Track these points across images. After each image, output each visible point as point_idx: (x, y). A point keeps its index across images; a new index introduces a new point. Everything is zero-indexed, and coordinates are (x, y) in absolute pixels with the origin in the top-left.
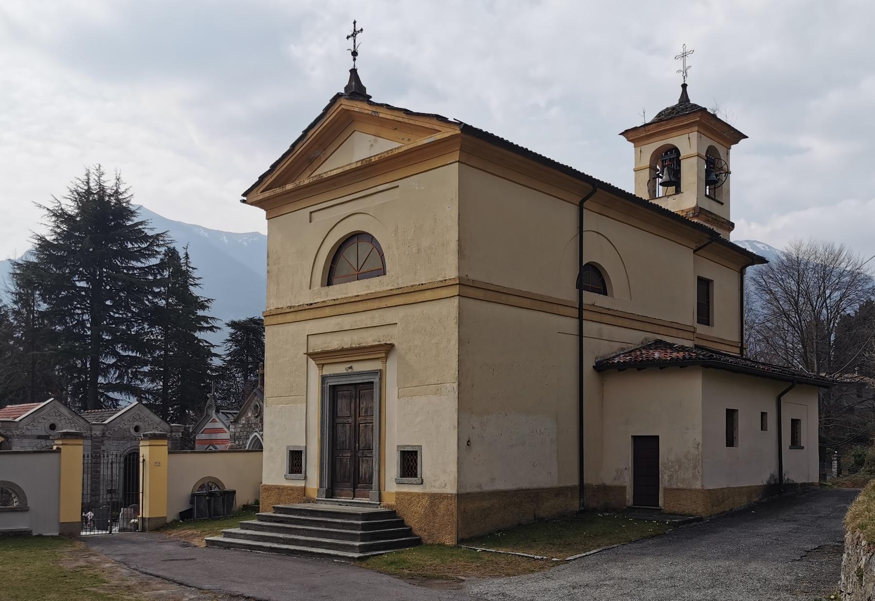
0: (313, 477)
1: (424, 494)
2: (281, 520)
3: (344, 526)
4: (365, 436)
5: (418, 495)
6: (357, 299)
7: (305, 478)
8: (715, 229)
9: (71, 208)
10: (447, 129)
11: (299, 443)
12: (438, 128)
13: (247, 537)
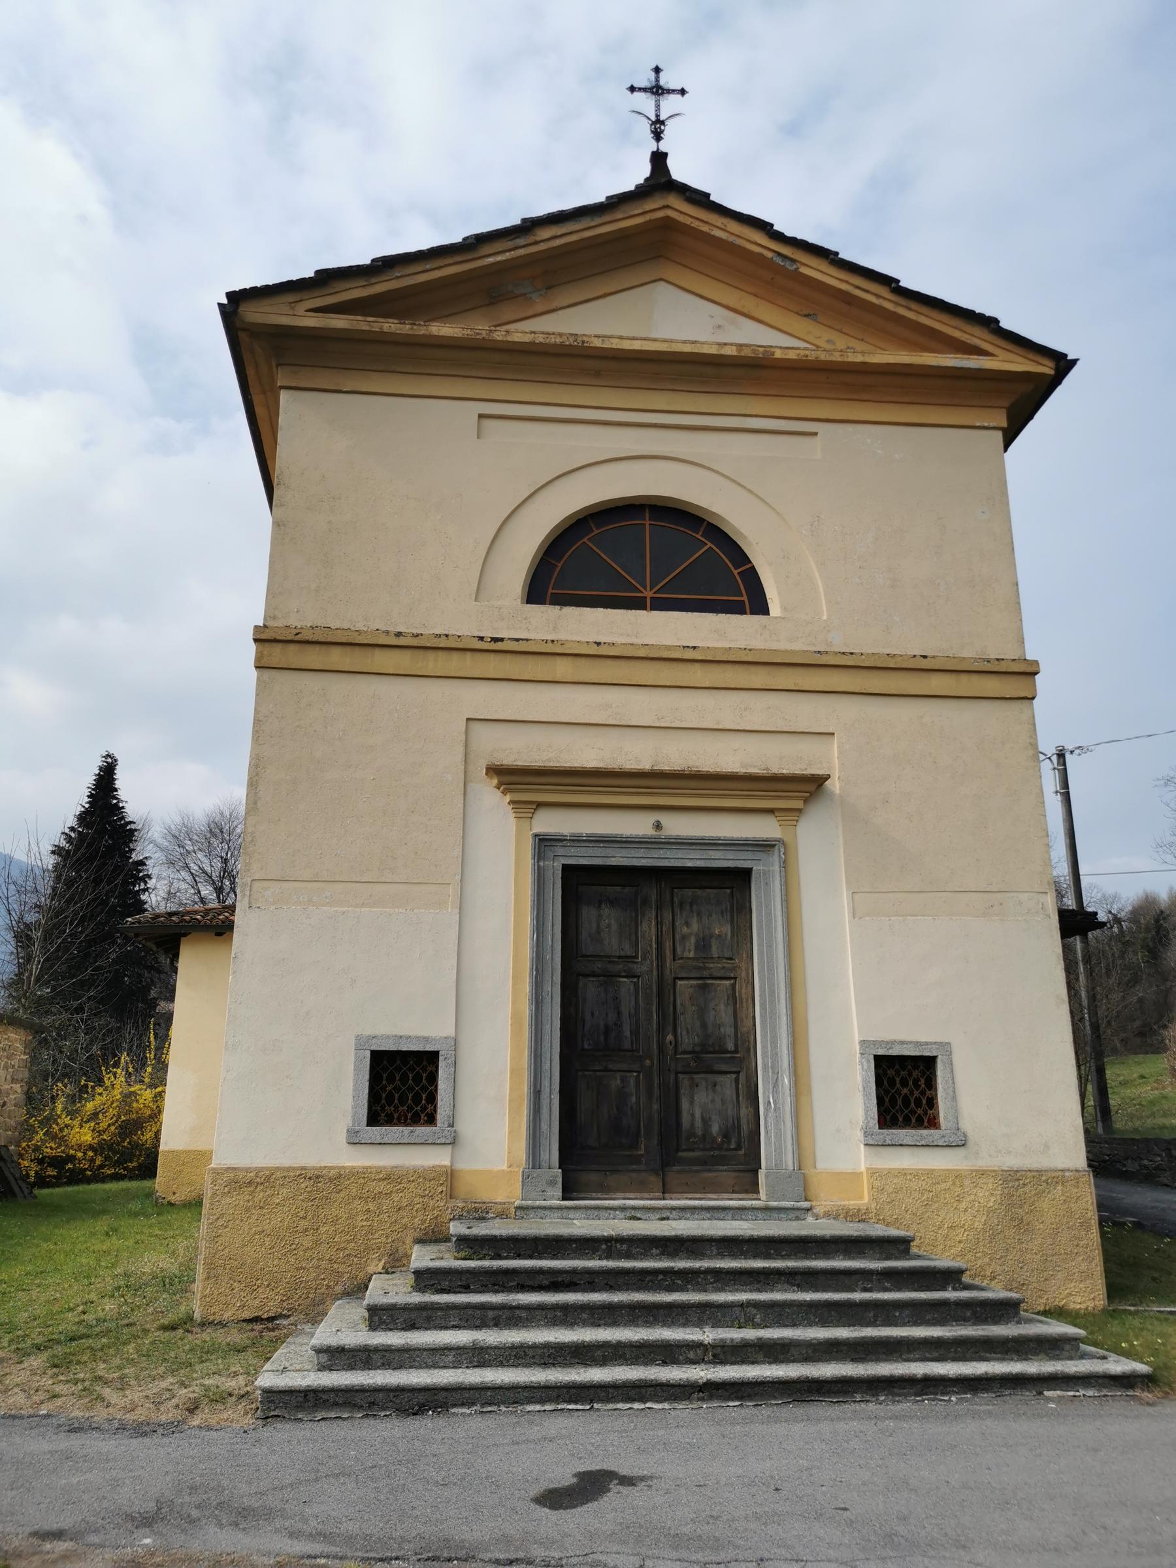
0: (493, 1130)
1: (983, 1173)
4: (702, 1012)
5: (958, 1176)
6: (924, 664)
7: (454, 1142)
8: (836, 755)
9: (225, 301)
13: (479, 1356)
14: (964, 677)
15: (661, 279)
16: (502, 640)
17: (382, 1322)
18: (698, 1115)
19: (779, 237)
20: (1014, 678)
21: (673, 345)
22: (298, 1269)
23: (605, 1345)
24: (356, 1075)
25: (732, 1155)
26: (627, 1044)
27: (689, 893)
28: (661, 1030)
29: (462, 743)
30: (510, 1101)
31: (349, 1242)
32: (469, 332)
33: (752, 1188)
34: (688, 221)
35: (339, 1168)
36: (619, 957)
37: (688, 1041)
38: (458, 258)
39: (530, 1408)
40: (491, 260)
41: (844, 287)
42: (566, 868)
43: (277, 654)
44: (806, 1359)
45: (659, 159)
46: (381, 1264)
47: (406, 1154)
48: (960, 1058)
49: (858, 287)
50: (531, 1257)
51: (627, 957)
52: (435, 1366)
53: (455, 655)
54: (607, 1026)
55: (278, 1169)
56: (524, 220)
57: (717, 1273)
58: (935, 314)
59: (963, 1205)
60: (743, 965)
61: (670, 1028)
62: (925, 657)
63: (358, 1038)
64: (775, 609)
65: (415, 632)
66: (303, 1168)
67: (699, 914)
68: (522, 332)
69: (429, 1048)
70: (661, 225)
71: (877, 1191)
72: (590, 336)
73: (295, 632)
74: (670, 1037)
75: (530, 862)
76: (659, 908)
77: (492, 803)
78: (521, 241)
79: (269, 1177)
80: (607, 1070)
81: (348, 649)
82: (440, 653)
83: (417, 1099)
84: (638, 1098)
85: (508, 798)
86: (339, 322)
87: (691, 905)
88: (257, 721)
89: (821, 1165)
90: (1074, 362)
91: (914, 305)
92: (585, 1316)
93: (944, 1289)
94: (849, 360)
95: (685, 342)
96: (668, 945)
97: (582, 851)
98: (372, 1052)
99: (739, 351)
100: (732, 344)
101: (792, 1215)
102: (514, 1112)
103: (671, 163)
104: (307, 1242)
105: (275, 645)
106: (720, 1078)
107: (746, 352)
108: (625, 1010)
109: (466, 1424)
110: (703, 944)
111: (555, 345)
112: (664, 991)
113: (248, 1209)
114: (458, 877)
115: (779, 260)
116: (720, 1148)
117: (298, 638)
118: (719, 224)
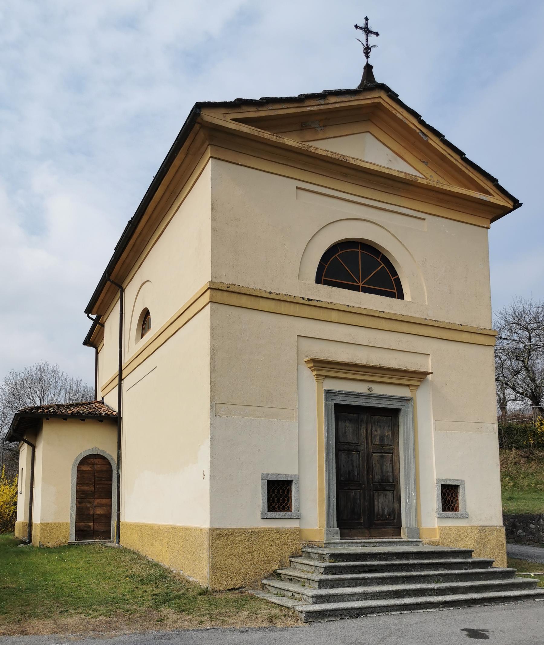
3: (382, 569)
5: (466, 529)
6: (381, 315)
11: (282, 470)
13: (365, 596)
14: (473, 335)
15: (369, 132)
17: (323, 586)
18: (380, 507)
19: (423, 123)
20: (490, 337)
21: (363, 163)
22: (247, 569)
24: (263, 490)
25: (391, 523)
26: (356, 479)
27: (377, 418)
28: (368, 474)
29: (296, 347)
30: (319, 501)
31: (265, 558)
32: (300, 145)
33: (399, 534)
34: (388, 107)
35: (259, 528)
36: (353, 443)
37: (377, 478)
38: (296, 105)
39: (393, 613)
41: (444, 153)
42: (336, 405)
44: (463, 593)
45: (368, 68)
46: (277, 566)
47: (280, 523)
49: (449, 154)
50: (354, 561)
51: (355, 443)
52: (351, 601)
53: (292, 305)
54: (349, 472)
56: (325, 91)
57: (422, 564)
58: (475, 173)
59: (467, 539)
60: (395, 448)
61: (371, 473)
62: (461, 325)
63: (262, 474)
64: (407, 296)
65: (277, 292)
66: (246, 529)
67: (380, 427)
68: (291, 141)
71: (441, 534)
72: (349, 157)
73: (227, 286)
74: (371, 476)
75: (323, 402)
76: (367, 423)
77: (308, 376)
78: (322, 102)
79: (233, 532)
80: (349, 489)
81: (249, 297)
82: (286, 303)
83: (284, 500)
84: (360, 500)
85: (315, 373)
86: (245, 129)
87: (378, 422)
88: (212, 328)
90: (521, 205)
91: (469, 167)
92: (388, 581)
93: (487, 568)
94: (445, 188)
95: (386, 168)
96: (370, 439)
97: (341, 398)
98: (268, 480)
99: (406, 176)
100: (403, 172)
101: (415, 544)
102: (321, 506)
103: (374, 70)
104: (249, 558)
105: (218, 291)
107: (408, 177)
109: (372, 620)
110: (382, 439)
111: (335, 159)
112: (369, 457)
113: (226, 545)
114: (297, 407)
115: (420, 134)
117: (228, 289)
118: (400, 111)
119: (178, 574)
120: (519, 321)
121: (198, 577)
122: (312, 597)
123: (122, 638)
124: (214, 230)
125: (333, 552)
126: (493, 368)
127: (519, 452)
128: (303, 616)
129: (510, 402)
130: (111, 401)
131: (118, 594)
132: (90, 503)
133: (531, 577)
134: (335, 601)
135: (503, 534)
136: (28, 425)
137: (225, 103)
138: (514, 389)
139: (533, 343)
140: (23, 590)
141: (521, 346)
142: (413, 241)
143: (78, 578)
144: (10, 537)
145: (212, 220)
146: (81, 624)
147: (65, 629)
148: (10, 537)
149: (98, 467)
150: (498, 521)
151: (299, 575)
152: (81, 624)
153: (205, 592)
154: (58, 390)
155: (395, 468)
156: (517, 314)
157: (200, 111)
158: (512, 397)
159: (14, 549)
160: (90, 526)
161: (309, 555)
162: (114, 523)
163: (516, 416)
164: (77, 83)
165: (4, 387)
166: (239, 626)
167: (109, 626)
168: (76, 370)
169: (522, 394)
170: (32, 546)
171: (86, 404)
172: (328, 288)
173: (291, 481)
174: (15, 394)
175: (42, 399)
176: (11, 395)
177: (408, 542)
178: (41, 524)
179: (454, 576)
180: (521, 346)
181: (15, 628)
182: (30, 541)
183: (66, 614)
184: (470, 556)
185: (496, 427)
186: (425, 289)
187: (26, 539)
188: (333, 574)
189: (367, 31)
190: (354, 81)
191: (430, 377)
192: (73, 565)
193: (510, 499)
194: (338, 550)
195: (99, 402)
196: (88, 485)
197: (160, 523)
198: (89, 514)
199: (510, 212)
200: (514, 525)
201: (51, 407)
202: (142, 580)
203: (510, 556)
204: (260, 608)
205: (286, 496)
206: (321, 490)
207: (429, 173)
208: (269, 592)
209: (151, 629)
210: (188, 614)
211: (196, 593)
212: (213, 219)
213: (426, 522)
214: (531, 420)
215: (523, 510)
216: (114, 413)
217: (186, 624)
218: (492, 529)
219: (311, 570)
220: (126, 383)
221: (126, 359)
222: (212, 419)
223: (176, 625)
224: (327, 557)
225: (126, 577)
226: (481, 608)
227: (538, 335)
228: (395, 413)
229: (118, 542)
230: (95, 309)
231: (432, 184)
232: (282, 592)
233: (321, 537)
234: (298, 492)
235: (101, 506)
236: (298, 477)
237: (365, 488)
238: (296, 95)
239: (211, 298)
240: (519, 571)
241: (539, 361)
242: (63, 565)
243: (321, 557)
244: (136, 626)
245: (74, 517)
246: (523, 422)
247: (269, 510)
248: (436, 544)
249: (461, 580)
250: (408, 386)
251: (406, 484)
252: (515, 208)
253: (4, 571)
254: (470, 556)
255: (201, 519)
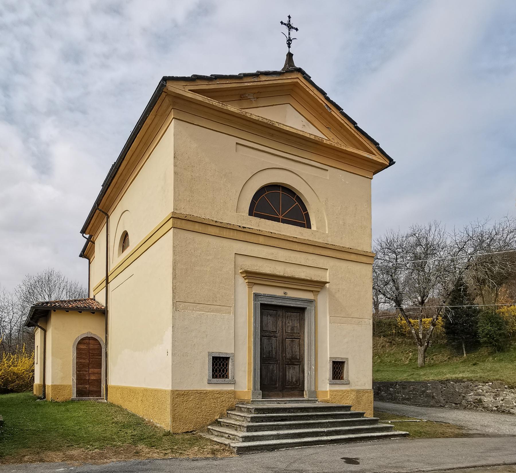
1: (353, 390)
2: (262, 419)
4: (292, 348)
6: (295, 240)
10: (378, 156)
11: (222, 349)
12: (374, 152)
13: (278, 437)
16: (245, 228)
17: (250, 430)
19: (328, 99)
23: (305, 433)
25: (297, 387)
27: (289, 313)
33: (302, 395)
34: (303, 85)
37: (289, 356)
40: (246, 84)
41: (342, 122)
43: (179, 223)
44: (344, 434)
45: (290, 56)
48: (350, 362)
55: (190, 390)
57: (317, 415)
63: (209, 352)
64: (314, 227)
68: (232, 108)
69: (227, 356)
70: (290, 83)
77: (242, 283)
78: (256, 79)
85: (247, 281)
86: (199, 97)
88: (174, 247)
89: (319, 389)
95: (301, 131)
96: (284, 328)
97: (265, 299)
106: (296, 366)
107: (317, 139)
108: (273, 347)
110: (292, 329)
112: (283, 341)
115: (326, 107)
116: (295, 385)
117: (185, 218)
119: (149, 422)
120: (389, 247)
121: (163, 424)
122: (242, 437)
123: (111, 464)
124: (175, 173)
125: (257, 407)
126: (371, 280)
127: (385, 339)
128: (235, 450)
129: (381, 304)
130: (100, 298)
131: (108, 434)
132: (86, 371)
133: (389, 424)
134: (257, 440)
135: (372, 395)
136: (40, 315)
137: (185, 77)
138: (384, 295)
139: (399, 263)
140: (41, 431)
141: (391, 264)
142: (317, 184)
143: (79, 423)
144: (30, 394)
145: (174, 166)
146: (82, 455)
147: (71, 458)
148: (30, 394)
149: (91, 346)
150: (369, 386)
151: (233, 423)
152: (82, 455)
153: (168, 434)
154: (61, 290)
155: (301, 349)
156: (389, 241)
157: (166, 83)
158: (383, 300)
159: (33, 403)
160: (86, 388)
161: (240, 410)
162: (103, 386)
163: (385, 313)
164: (73, 55)
165: (22, 287)
166: (192, 456)
167: (102, 456)
168: (74, 276)
169: (389, 298)
170: (46, 401)
171: (82, 301)
172: (258, 219)
173: (229, 358)
174: (31, 292)
175: (50, 296)
176: (27, 293)
177: (308, 400)
178: (52, 386)
179: (339, 423)
180: (391, 264)
181: (35, 457)
182: (45, 397)
183: (71, 448)
184: (349, 410)
185: (371, 321)
186: (326, 221)
187: (41, 395)
188: (257, 422)
189: (290, 26)
190: (279, 66)
191: (327, 285)
192: (76, 414)
193: (378, 371)
194: (260, 406)
195: (92, 299)
196: (84, 359)
197: (136, 386)
198: (85, 379)
199: (387, 167)
200: (379, 389)
201: (57, 302)
202: (124, 426)
203: (376, 409)
204: (206, 445)
205: (225, 368)
206: (249, 364)
207: (331, 136)
208: (212, 434)
209: (131, 458)
210: (156, 449)
211: (161, 435)
212: (175, 166)
213: (322, 387)
214: (395, 317)
215: (385, 379)
216: (103, 307)
217: (155, 455)
218: (365, 391)
219: (241, 418)
220: (111, 286)
221: (111, 268)
222: (173, 313)
223: (148, 455)
224: (253, 411)
225: (113, 423)
226: (355, 444)
227: (402, 257)
228: (302, 310)
229: (107, 399)
230: (88, 231)
231: (333, 144)
232: (221, 435)
233: (249, 397)
234: (233, 365)
235: (94, 374)
236: (234, 355)
237: (280, 363)
238: (236, 73)
239: (173, 224)
240: (381, 419)
241: (402, 275)
242: (69, 414)
243: (249, 411)
244: (120, 456)
245: (75, 381)
246: (389, 318)
247: (213, 378)
248: (327, 401)
249: (342, 426)
250: (312, 291)
251: (308, 361)
252: (390, 165)
253: (27, 418)
254: (349, 410)
255: (165, 384)
